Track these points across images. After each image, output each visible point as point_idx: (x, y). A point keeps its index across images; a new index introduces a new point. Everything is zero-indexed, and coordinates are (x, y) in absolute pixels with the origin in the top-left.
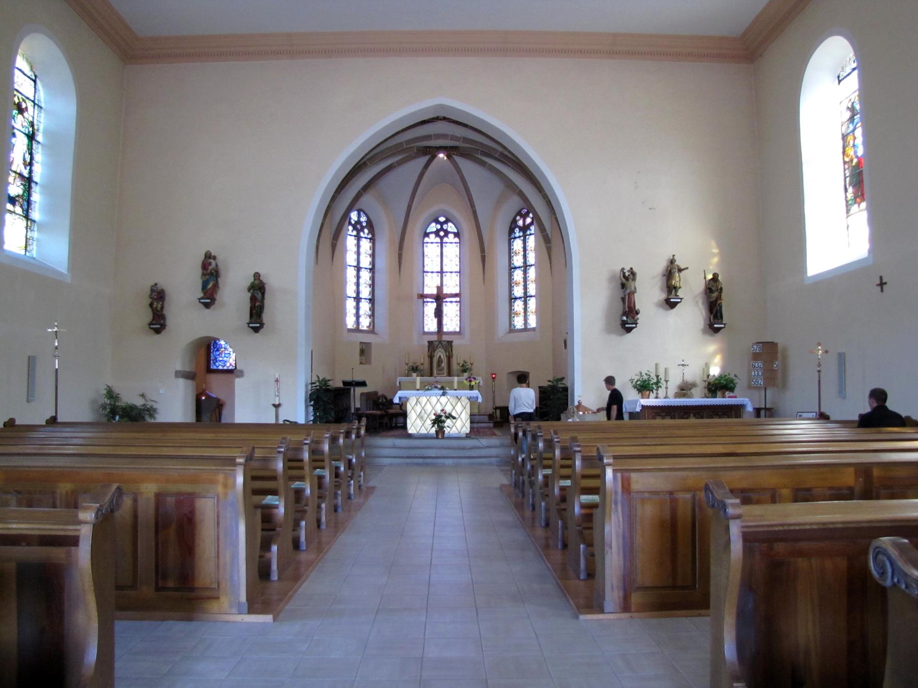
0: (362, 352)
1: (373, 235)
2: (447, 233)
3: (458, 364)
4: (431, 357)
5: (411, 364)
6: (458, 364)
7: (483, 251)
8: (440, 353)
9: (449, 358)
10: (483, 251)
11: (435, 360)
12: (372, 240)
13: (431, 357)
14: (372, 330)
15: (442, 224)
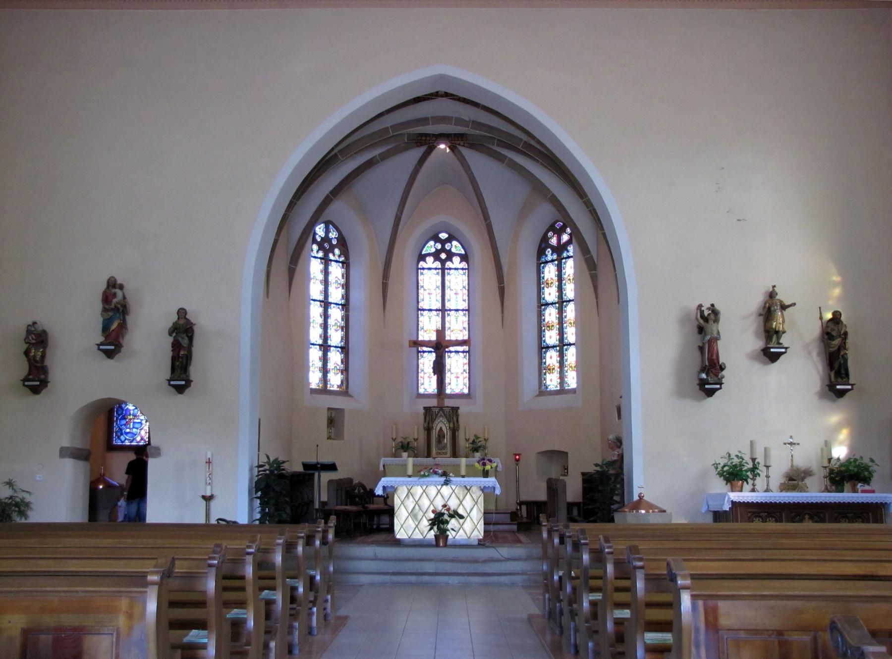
0: (331, 422)
1: (347, 258)
2: (450, 255)
3: (467, 440)
4: (428, 430)
5: (399, 440)
6: (467, 440)
7: (500, 279)
8: (441, 424)
9: (454, 431)
10: (500, 279)
11: (434, 434)
12: (346, 264)
13: (428, 430)
14: (345, 390)
15: (443, 250)
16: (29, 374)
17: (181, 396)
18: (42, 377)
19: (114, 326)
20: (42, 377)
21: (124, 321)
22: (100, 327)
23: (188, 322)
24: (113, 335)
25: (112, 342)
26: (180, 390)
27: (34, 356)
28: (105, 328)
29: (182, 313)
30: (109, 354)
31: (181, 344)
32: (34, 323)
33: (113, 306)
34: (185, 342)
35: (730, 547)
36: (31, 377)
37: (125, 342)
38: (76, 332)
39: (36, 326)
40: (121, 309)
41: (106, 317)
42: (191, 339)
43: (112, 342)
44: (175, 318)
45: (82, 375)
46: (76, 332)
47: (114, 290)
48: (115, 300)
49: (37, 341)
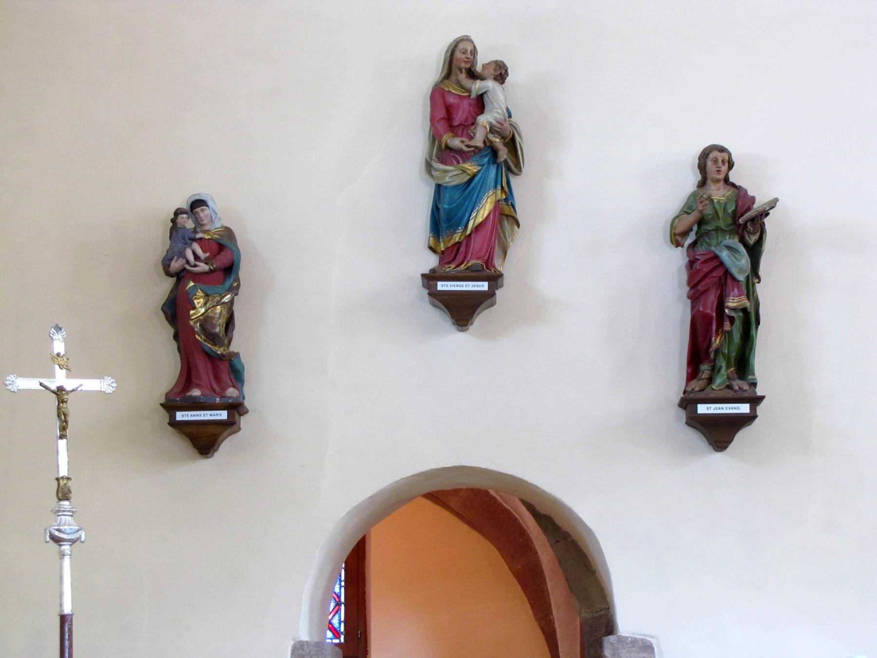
16: (187, 378)
17: (719, 456)
18: (231, 392)
19: (484, 210)
20: (231, 392)
21: (509, 198)
22: (509, 71)
23: (742, 199)
24: (477, 244)
25: (467, 261)
26: (720, 433)
27: (206, 321)
28: (442, 220)
29: (713, 163)
30: (462, 311)
31: (727, 273)
32: (198, 204)
33: (478, 141)
34: (737, 263)
35: (453, 255)
36: (196, 393)
37: (507, 267)
38: (330, 230)
39: (203, 213)
40: (504, 154)
41: (452, 175)
42: (755, 252)
43: (467, 261)
44: (690, 180)
45: (361, 398)
46: (330, 230)
47: (477, 86)
48: (484, 120)
49: (200, 274)
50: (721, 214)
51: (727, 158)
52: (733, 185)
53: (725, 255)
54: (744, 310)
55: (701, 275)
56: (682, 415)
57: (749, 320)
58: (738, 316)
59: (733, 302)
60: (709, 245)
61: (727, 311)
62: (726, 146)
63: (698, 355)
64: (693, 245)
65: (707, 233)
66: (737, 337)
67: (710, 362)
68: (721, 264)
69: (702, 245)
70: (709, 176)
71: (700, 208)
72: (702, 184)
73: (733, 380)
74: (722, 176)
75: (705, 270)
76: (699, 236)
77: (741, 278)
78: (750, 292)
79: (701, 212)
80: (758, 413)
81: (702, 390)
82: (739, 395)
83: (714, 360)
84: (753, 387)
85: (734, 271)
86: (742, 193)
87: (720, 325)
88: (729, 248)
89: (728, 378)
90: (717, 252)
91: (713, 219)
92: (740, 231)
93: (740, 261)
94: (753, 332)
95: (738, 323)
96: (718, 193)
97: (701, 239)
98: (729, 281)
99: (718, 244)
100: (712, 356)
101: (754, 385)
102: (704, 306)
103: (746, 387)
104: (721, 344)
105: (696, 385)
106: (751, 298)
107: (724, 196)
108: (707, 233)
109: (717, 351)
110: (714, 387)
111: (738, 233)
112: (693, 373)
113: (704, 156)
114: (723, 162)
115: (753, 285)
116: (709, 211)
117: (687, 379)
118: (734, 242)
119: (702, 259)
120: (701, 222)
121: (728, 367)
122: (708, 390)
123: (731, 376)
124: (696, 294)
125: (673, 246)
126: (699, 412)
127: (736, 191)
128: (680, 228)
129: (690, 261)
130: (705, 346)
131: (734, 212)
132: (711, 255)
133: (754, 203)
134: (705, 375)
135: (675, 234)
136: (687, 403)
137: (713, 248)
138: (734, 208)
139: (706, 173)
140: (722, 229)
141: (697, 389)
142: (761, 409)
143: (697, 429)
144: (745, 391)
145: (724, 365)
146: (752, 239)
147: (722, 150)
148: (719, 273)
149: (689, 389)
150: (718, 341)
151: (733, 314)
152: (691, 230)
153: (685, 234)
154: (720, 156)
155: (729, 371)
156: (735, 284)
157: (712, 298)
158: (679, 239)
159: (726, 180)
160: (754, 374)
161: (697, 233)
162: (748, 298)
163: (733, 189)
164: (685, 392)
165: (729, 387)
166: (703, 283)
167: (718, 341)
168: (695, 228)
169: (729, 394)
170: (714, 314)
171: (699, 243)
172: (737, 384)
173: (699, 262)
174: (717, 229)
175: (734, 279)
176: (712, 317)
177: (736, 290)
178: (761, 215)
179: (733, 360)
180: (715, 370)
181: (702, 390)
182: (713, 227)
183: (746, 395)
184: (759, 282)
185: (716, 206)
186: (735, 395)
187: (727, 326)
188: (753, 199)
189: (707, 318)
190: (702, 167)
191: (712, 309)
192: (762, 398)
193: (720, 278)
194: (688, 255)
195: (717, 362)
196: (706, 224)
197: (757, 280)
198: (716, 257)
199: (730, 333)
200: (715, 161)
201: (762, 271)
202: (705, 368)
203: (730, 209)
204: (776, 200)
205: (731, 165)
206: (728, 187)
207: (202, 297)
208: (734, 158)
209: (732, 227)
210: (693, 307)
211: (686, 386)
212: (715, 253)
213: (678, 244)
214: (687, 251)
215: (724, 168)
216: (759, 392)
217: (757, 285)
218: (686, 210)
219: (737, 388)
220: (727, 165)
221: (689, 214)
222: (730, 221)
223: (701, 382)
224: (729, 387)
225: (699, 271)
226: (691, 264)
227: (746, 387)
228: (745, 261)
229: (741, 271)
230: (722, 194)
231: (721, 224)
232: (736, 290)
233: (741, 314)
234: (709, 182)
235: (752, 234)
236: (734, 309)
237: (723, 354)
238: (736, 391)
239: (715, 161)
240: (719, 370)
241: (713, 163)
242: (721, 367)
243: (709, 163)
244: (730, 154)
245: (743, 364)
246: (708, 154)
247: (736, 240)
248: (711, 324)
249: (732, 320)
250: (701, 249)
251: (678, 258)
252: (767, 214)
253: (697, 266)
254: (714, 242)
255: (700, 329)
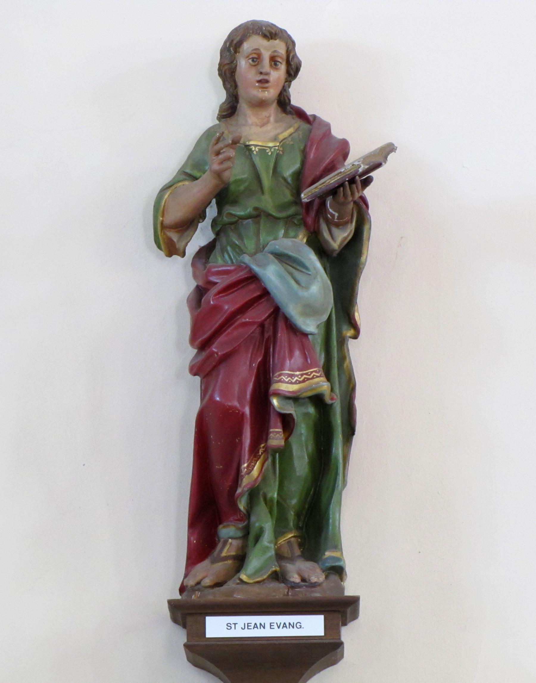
29: (255, 64)
31: (277, 312)
42: (344, 267)
50: (267, 181)
51: (282, 51)
52: (300, 114)
53: (271, 274)
54: (318, 400)
55: (219, 319)
56: (180, 636)
57: (331, 423)
58: (304, 416)
59: (288, 382)
60: (240, 251)
61: (275, 402)
62: (281, 25)
63: (211, 507)
64: (206, 252)
65: (236, 224)
66: (301, 463)
67: (241, 520)
68: (265, 293)
69: (223, 250)
70: (241, 92)
71: (216, 167)
72: (230, 111)
73: (291, 560)
74: (271, 93)
75: (228, 308)
76: (220, 228)
77: (310, 326)
78: (335, 362)
79: (218, 174)
80: (343, 639)
81: (218, 585)
82: (302, 594)
83: (249, 514)
84: (334, 578)
85: (293, 311)
86: (318, 133)
87: (260, 434)
88: (282, 258)
89: (279, 557)
90: (256, 269)
91: (249, 193)
92: (310, 220)
93: (307, 288)
94: (338, 449)
95: (303, 431)
96: (263, 133)
97: (224, 240)
98: (282, 335)
99: (260, 249)
100: (242, 505)
101: (338, 571)
102: (225, 391)
103: (317, 576)
104: (264, 476)
105: (208, 571)
106: (335, 372)
107: (275, 139)
108: (236, 224)
109: (254, 494)
110: (244, 577)
111: (306, 225)
112: (202, 545)
113: (233, 45)
114: (274, 60)
115: (342, 342)
116: (238, 172)
117: (189, 558)
118: (297, 244)
119: (221, 282)
120: (223, 196)
121: (278, 533)
122: (231, 585)
123: (286, 551)
124: (209, 360)
125: (162, 254)
126: (208, 635)
127: (306, 126)
128: (175, 214)
129: (198, 287)
130: (228, 483)
131: (298, 175)
132: (242, 274)
133: (345, 156)
134: (229, 549)
135: (164, 227)
136: (187, 612)
137: (247, 259)
138: (297, 166)
139: (236, 86)
140: (268, 215)
141: (207, 582)
142: (348, 634)
143: (214, 674)
144: (314, 585)
145: (268, 526)
146: (337, 239)
147: (271, 33)
148: (259, 314)
149: (191, 582)
150: (255, 472)
151: (290, 409)
152: (202, 216)
153: (187, 225)
154: (267, 48)
155: (281, 541)
156: (295, 340)
157: (244, 370)
158: (174, 236)
159: (283, 102)
160: (337, 547)
161: (214, 223)
162: (328, 375)
163: (298, 123)
164: (182, 589)
165: (278, 577)
166: (222, 338)
167: (255, 472)
168: (212, 212)
169: (278, 592)
170: (247, 410)
171: (218, 247)
172: (297, 569)
173: (214, 290)
174: (258, 215)
175: (293, 329)
176: (243, 415)
177: (297, 353)
178: (352, 181)
179: (291, 515)
180: (249, 537)
181: (218, 585)
182: (249, 210)
183: (317, 594)
184: (355, 337)
185: (257, 161)
186: (291, 596)
187: (276, 437)
188: (343, 149)
189: (231, 420)
190: (228, 72)
191: (241, 399)
192: (354, 602)
193: (262, 325)
194: (195, 276)
195: (253, 519)
196: (235, 202)
197: (350, 332)
198: (253, 278)
199: (284, 453)
200: (256, 59)
201: (362, 312)
202: (228, 532)
203: (289, 169)
204: (390, 148)
205: (293, 70)
206: (289, 118)
207: (277, 394)
208: (300, 51)
209: (292, 210)
210: (204, 392)
211: (186, 576)
212: (251, 270)
213: (172, 250)
214: (193, 265)
215: (278, 75)
216: (350, 588)
217: (352, 344)
218: (188, 173)
219: (296, 579)
220: (283, 67)
221: (195, 178)
222: (288, 196)
223: (219, 566)
224: (278, 577)
225: (216, 309)
226: (200, 292)
227: (317, 576)
228: (318, 286)
229: (310, 310)
230: (272, 134)
231: (267, 203)
232: (297, 353)
233: (311, 410)
234: (243, 106)
235: (337, 225)
236: (295, 399)
237: (268, 502)
238: (293, 586)
239: (256, 59)
240: (257, 539)
241: (255, 64)
242: (261, 532)
243: (243, 64)
244: (290, 44)
245: (313, 524)
246: (239, 44)
247: (302, 238)
248: (239, 433)
249: (287, 422)
250: (219, 261)
251: (175, 279)
252: (367, 182)
253: (211, 298)
254: (250, 245)
255: (215, 443)
